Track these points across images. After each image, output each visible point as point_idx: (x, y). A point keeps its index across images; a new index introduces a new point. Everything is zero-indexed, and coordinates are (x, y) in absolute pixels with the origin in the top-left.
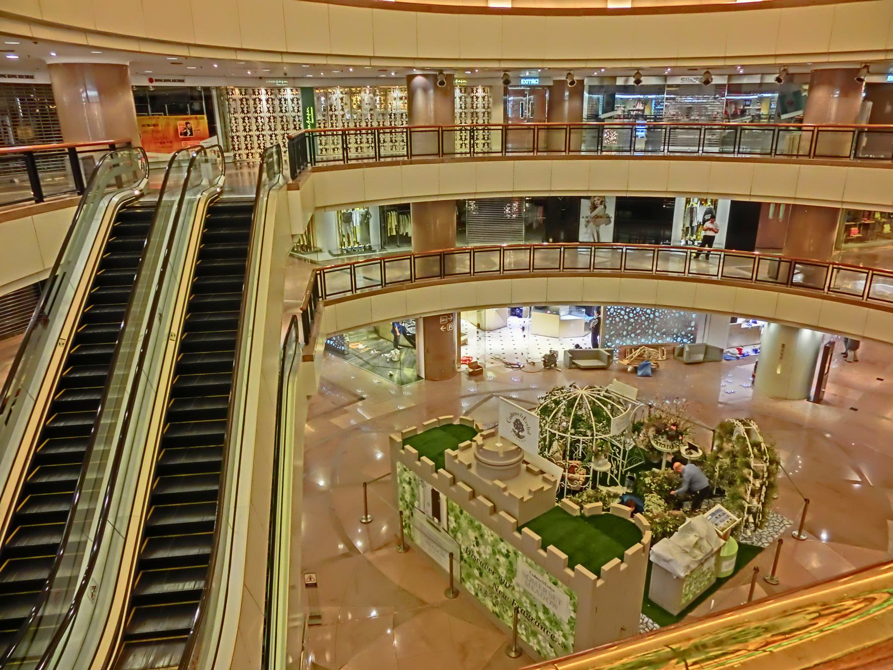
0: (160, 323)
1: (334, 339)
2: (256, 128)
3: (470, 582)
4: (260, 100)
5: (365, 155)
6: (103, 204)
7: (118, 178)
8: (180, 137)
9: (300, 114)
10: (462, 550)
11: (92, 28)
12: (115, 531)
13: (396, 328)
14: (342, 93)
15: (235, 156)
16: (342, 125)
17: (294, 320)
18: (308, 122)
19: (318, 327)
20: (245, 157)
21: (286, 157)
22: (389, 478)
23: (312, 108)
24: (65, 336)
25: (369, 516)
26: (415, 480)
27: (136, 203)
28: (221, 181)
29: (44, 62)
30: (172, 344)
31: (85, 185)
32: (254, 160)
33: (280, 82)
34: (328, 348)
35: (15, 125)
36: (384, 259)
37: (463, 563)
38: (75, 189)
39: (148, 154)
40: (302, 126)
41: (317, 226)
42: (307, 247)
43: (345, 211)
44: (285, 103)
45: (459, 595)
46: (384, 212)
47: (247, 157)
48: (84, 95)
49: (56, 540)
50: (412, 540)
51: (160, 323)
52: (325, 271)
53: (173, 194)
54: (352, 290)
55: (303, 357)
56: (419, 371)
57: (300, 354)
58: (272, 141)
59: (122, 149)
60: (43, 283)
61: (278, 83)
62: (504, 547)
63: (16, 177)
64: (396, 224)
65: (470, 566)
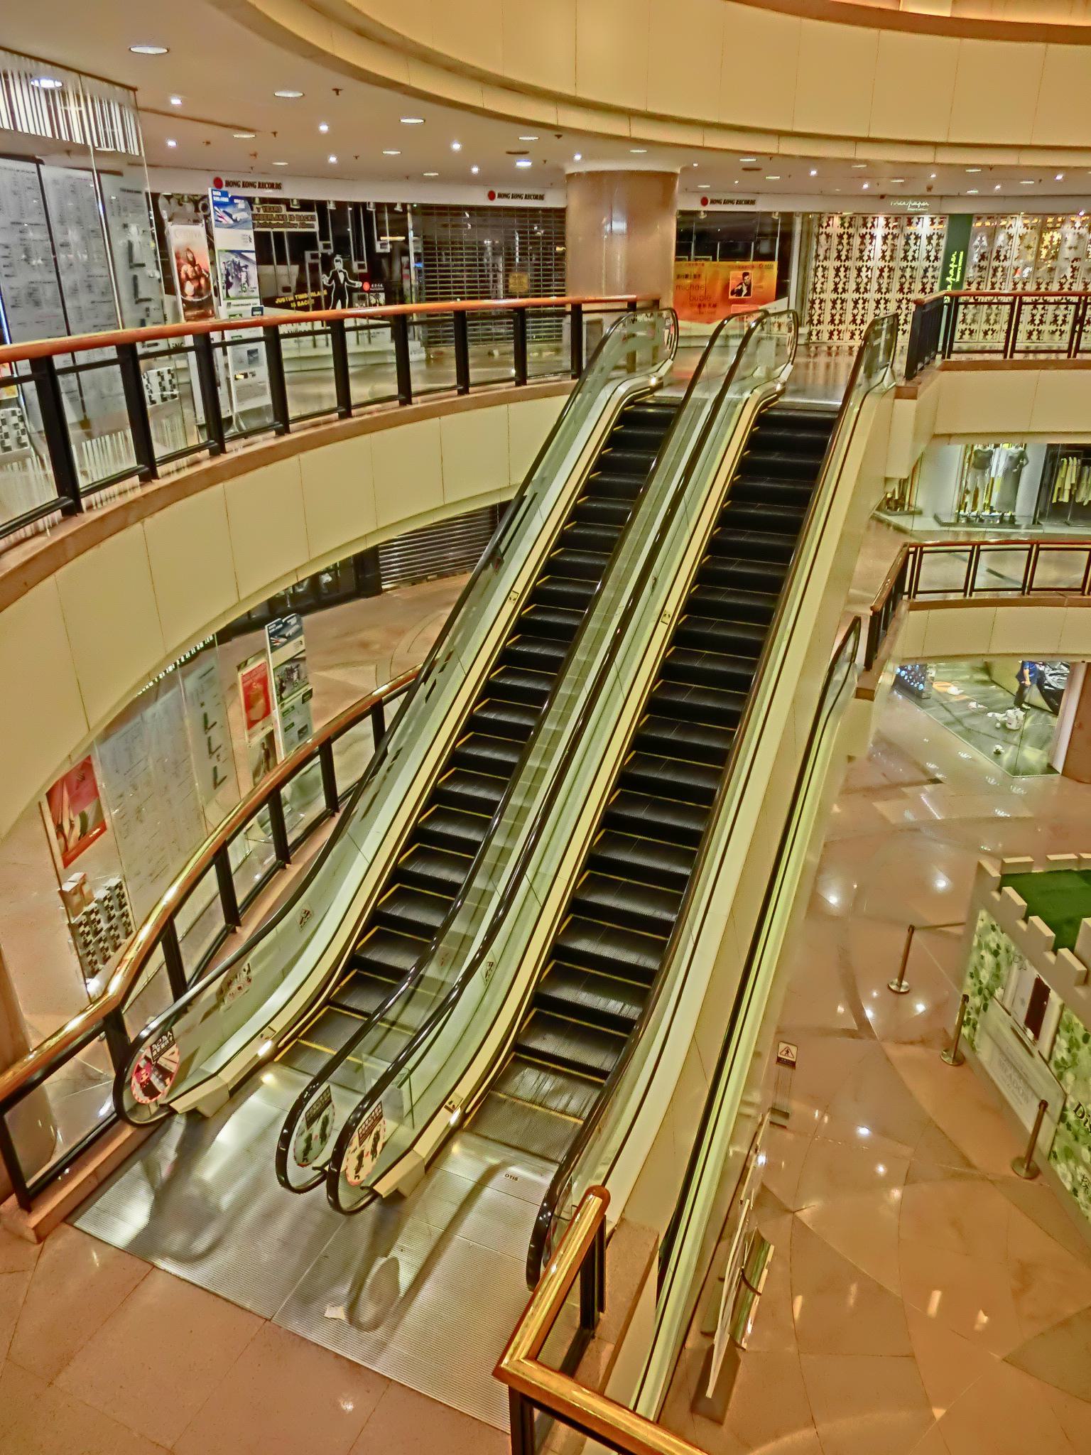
0: (652, 591)
1: (909, 668)
2: (854, 287)
3: (1068, 1165)
4: (872, 237)
5: (1043, 346)
6: (605, 394)
7: (632, 357)
8: (730, 297)
9: (939, 264)
10: (1068, 1105)
11: (640, 107)
12: (532, 891)
13: (1026, 671)
14: (1025, 225)
15: (810, 334)
16: (1011, 286)
17: (855, 625)
18: (949, 279)
19: (892, 644)
20: (825, 336)
21: (903, 340)
22: (958, 931)
23: (962, 253)
24: (519, 588)
25: (905, 983)
26: (1007, 951)
27: (649, 399)
28: (785, 372)
29: (561, 170)
30: (662, 628)
31: (584, 366)
32: (840, 343)
33: (915, 204)
34: (899, 683)
35: (508, 272)
36: (1038, 544)
37: (1062, 1126)
38: (570, 368)
39: (681, 323)
40: (936, 287)
41: (925, 468)
42: (897, 504)
43: (980, 447)
44: (915, 244)
45: (1040, 1178)
46: (1055, 457)
47: (830, 338)
48: (608, 228)
49: (457, 877)
50: (974, 1049)
51: (652, 591)
52: (925, 549)
53: (708, 389)
54: (965, 591)
55: (858, 690)
56: (1052, 754)
57: (852, 684)
58: (877, 312)
59: (643, 310)
60: (508, 503)
61: (911, 206)
63: (496, 347)
64: (1074, 481)
65: (1076, 1139)
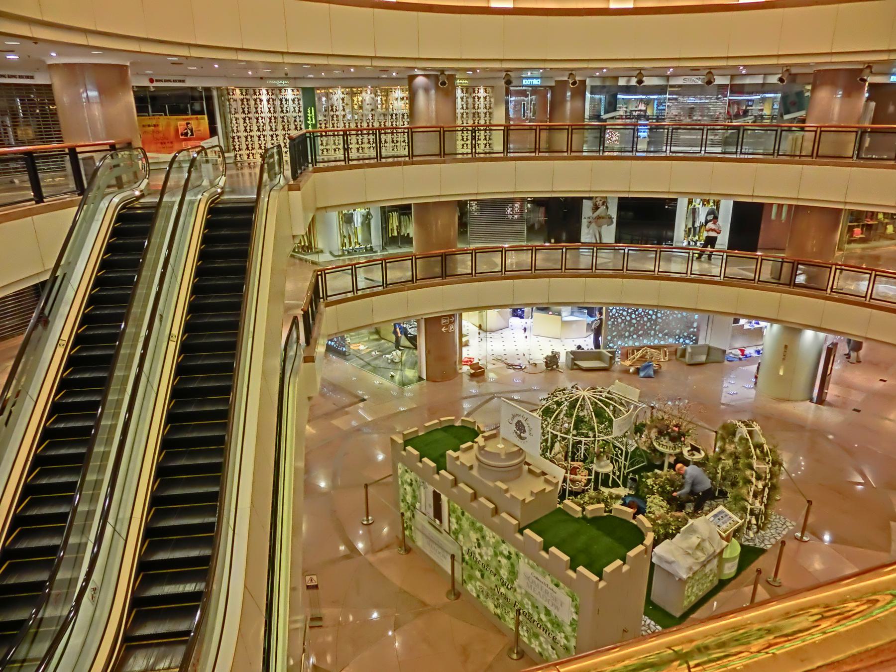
0: (161, 324)
1: (335, 340)
2: (256, 128)
3: (472, 584)
4: (261, 100)
5: (366, 156)
6: (104, 204)
7: (119, 179)
8: (181, 137)
9: (302, 114)
10: (464, 552)
11: (92, 28)
12: (116, 533)
13: (398, 329)
14: (343, 93)
15: (236, 156)
16: (343, 125)
17: (295, 321)
18: (309, 122)
19: (319, 328)
20: (245, 157)
21: (287, 158)
22: (390, 479)
23: (313, 108)
24: (65, 337)
25: (370, 518)
26: (416, 481)
27: (137, 204)
28: (222, 181)
29: (44, 62)
30: (172, 345)
31: (86, 186)
32: (254, 161)
33: (281, 82)
34: (329, 349)
35: (15, 125)
36: (385, 260)
37: (464, 564)
38: (75, 189)
39: (148, 154)
40: (303, 126)
41: (318, 227)
42: (308, 248)
43: (346, 212)
44: (286, 104)
45: (461, 597)
46: (385, 213)
47: (248, 158)
48: (84, 95)
49: (56, 541)
50: (414, 541)
51: (161, 324)
52: (326, 271)
53: (173, 195)
54: (353, 291)
55: (304, 358)
56: (420, 372)
57: (301, 355)
58: (273, 142)
59: (122, 149)
60: (44, 283)
61: (279, 83)
63: (16, 178)
64: (397, 224)
65: (472, 568)
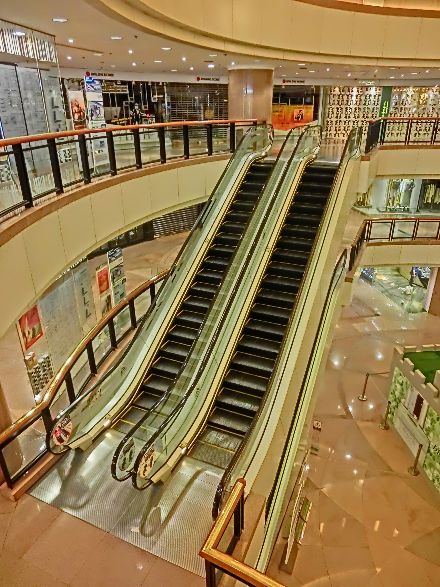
0: (263, 239)
1: (367, 269)
2: (345, 116)
3: (431, 470)
4: (352, 96)
5: (421, 140)
6: (244, 159)
7: (255, 144)
8: (295, 120)
9: (379, 106)
10: (431, 446)
11: (258, 43)
12: (214, 360)
13: (414, 271)
14: (414, 91)
15: (327, 135)
16: (408, 115)
17: (345, 252)
18: (383, 113)
19: (360, 260)
20: (333, 136)
21: (364, 137)
22: (386, 375)
23: (388, 102)
24: (209, 237)
25: (365, 397)
26: (406, 384)
27: (262, 161)
28: (317, 150)
29: (226, 69)
30: (267, 253)
31: (236, 148)
32: (339, 138)
33: (369, 82)
34: (363, 276)
35: (205, 110)
36: (419, 220)
37: (428, 454)
38: (230, 148)
39: (275, 130)
40: (378, 116)
41: (373, 189)
42: (362, 203)
43: (395, 180)
44: (369, 98)
45: (419, 475)
46: (425, 184)
47: (335, 136)
48: (245, 92)
49: (184, 354)
50: (393, 423)
51: (263, 239)
52: (373, 221)
53: (285, 157)
54: (389, 238)
55: (346, 278)
56: (424, 304)
57: (344, 276)
58: (354, 126)
59: (259, 125)
60: (205, 203)
61: (367, 83)
62: (401, 379)
63: (200, 140)
64: (433, 194)
65: (434, 459)
